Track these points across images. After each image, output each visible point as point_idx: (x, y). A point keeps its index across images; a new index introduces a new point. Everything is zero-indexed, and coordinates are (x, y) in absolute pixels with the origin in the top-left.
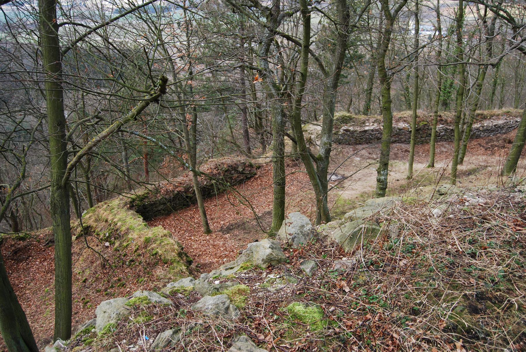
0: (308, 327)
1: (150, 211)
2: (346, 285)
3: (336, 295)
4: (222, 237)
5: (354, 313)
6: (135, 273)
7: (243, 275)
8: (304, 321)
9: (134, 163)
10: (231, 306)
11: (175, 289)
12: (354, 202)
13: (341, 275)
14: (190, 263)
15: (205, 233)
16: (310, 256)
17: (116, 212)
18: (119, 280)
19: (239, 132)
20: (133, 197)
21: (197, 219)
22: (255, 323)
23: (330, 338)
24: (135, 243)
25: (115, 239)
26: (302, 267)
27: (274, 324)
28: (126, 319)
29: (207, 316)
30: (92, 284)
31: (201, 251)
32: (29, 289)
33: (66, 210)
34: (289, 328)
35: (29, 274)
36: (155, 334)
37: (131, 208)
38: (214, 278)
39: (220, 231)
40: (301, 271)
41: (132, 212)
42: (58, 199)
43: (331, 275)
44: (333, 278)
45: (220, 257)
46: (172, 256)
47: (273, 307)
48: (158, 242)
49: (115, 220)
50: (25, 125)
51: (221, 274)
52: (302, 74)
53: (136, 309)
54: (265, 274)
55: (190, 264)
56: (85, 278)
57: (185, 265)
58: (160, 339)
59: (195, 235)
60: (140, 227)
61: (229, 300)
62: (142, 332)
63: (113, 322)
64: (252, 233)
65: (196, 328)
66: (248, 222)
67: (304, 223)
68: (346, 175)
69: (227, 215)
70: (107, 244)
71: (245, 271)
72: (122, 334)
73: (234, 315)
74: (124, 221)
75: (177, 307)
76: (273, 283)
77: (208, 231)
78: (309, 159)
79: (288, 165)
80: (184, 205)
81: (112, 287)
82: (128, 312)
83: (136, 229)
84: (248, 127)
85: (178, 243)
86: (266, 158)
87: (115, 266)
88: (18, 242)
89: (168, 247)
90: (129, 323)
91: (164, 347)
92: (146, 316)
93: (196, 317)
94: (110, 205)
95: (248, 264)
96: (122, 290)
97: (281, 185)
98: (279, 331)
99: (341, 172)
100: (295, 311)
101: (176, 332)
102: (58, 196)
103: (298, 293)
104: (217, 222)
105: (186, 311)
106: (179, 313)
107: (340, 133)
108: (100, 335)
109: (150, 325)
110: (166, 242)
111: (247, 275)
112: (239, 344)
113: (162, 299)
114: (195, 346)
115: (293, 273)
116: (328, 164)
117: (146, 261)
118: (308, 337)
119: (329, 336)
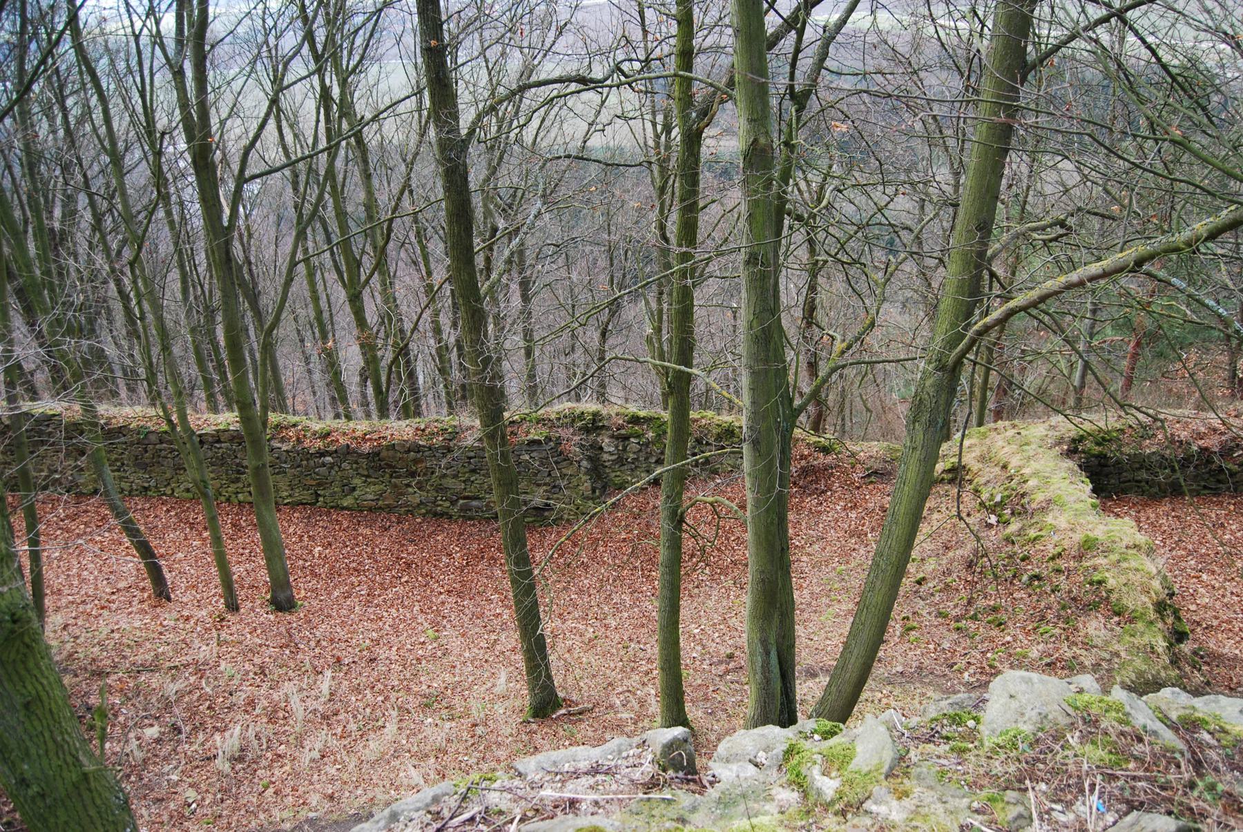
1: (1113, 475)
6: (1034, 608)
11: (1197, 715)
14: (1180, 636)
17: (1031, 453)
18: (995, 609)
21: (1233, 533)
24: (1056, 538)
25: (1013, 514)
28: (1058, 736)
30: (932, 595)
31: (1217, 618)
32: (809, 555)
33: (940, 421)
35: (817, 524)
36: (1124, 807)
37: (1071, 453)
41: (1070, 464)
42: (932, 391)
48: (1114, 557)
49: (1026, 471)
53: (1090, 724)
56: (922, 575)
57: (1164, 637)
59: (1213, 572)
60: (1079, 506)
62: (1093, 786)
63: (1027, 728)
70: (993, 519)
72: (1041, 766)
74: (1046, 481)
75: (1198, 765)
81: (974, 618)
82: (1068, 720)
83: (1068, 505)
85: (1165, 577)
89: (1136, 578)
90: (1063, 747)
92: (1111, 752)
94: (1023, 432)
102: (932, 386)
105: (1220, 787)
106: (1200, 784)
108: (988, 744)
109: (1114, 778)
110: (1133, 564)
117: (1070, 591)
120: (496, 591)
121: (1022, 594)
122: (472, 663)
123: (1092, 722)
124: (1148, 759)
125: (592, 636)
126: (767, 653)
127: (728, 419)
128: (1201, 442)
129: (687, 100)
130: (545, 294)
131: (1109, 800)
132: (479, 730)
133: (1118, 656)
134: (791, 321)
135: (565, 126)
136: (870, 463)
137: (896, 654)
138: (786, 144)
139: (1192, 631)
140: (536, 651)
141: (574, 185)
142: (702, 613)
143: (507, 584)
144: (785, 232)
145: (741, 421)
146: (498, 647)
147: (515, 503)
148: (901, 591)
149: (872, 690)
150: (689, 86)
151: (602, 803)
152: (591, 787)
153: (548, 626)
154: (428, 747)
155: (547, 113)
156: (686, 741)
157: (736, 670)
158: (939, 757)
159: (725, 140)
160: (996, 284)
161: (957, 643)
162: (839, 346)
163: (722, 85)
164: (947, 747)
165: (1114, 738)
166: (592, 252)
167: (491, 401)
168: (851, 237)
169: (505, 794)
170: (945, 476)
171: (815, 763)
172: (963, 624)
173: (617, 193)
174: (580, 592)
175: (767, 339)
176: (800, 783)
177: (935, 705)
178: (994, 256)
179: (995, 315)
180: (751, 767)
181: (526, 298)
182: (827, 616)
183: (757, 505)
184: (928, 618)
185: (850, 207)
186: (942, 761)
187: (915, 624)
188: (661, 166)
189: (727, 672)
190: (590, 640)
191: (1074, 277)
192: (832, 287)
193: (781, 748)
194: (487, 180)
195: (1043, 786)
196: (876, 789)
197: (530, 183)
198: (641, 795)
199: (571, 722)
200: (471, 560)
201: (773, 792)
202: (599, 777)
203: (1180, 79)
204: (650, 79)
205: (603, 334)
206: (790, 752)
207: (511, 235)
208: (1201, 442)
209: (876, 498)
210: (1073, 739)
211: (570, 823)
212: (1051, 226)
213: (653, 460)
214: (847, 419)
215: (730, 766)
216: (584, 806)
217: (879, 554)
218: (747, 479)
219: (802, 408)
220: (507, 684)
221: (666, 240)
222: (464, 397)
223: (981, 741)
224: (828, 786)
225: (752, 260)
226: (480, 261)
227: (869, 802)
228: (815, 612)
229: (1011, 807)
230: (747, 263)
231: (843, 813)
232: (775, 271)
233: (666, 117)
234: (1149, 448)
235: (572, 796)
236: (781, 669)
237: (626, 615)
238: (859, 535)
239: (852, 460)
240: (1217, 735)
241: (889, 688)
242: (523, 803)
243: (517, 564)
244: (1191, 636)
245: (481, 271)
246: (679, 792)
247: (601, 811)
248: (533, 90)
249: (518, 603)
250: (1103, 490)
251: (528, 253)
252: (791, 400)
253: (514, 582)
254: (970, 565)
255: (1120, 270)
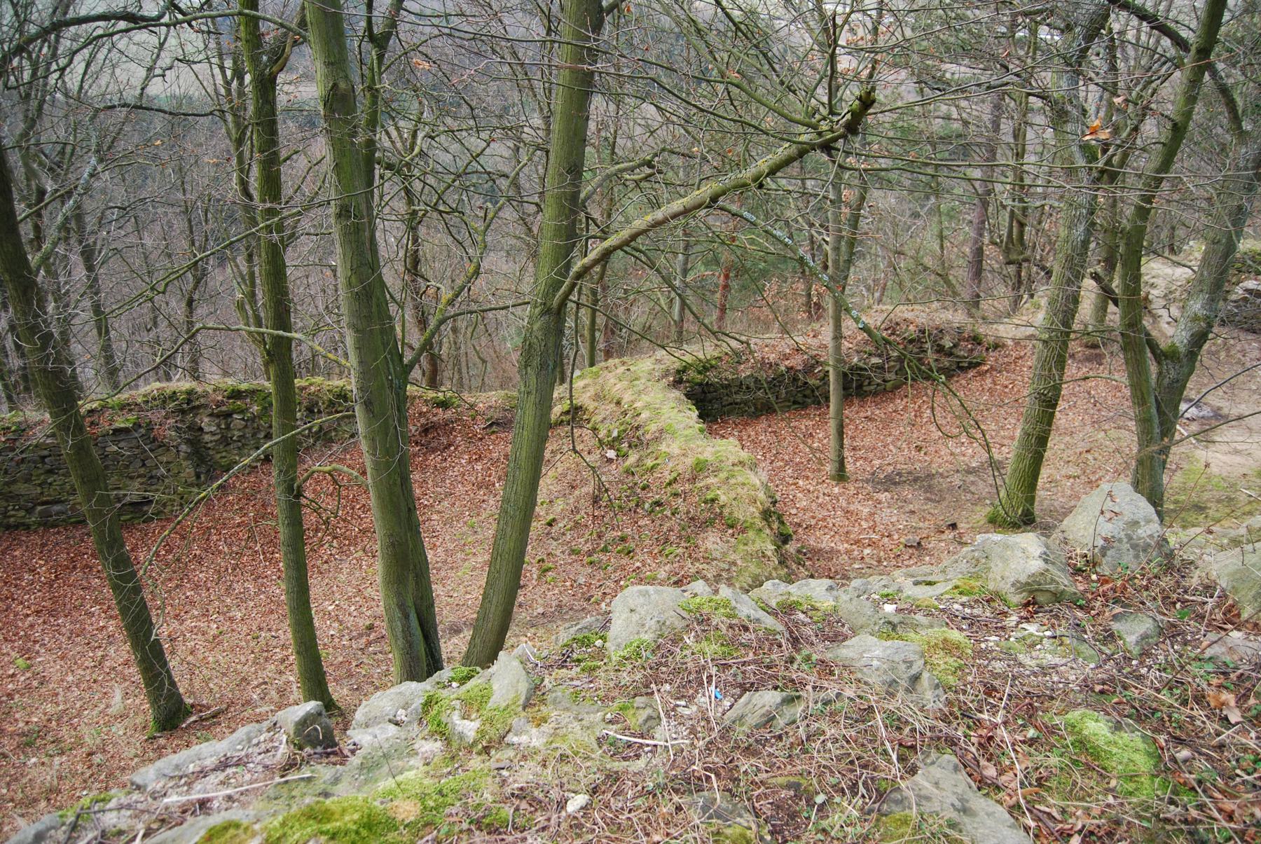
0: (1113, 783)
1: (714, 400)
2: (1233, 703)
3: (1198, 723)
4: (869, 497)
5: (1244, 783)
6: (658, 533)
7: (956, 606)
8: (1106, 763)
9: (702, 282)
10: (926, 675)
12: (1232, 486)
13: (1223, 673)
14: (785, 539)
15: (833, 478)
16: (1143, 603)
17: (642, 387)
18: (623, 539)
19: (959, 253)
20: (688, 358)
21: (820, 441)
22: (980, 732)
23: (1168, 827)
24: (671, 465)
25: (630, 446)
26: (1116, 626)
27: (1026, 747)
29: (866, 683)
30: (564, 534)
33: (551, 363)
34: (1062, 769)
35: (443, 481)
36: (738, 691)
37: (677, 383)
38: (882, 596)
39: (867, 481)
40: (1112, 635)
41: (677, 394)
42: (540, 335)
43: (1193, 668)
44: (1198, 676)
45: (857, 542)
46: (748, 513)
47: (1029, 707)
48: (723, 475)
49: (638, 404)
50: (488, 163)
51: (900, 590)
52: (1175, 125)
54: (1015, 618)
55: (785, 542)
56: (551, 517)
58: (750, 706)
59: (807, 478)
61: (922, 661)
63: (648, 637)
64: (945, 504)
65: (839, 705)
66: (941, 475)
67: (1140, 516)
68: (1225, 411)
69: (891, 447)
70: (611, 454)
71: (964, 599)
72: (664, 669)
73: (932, 699)
74: (657, 412)
75: (795, 641)
76: (1033, 645)
77: (841, 475)
78: (1142, 352)
79: (1072, 356)
80: (795, 402)
81: (605, 550)
82: (684, 623)
84: (986, 241)
86: (1022, 324)
87: (620, 507)
88: (435, 410)
89: (742, 492)
91: (757, 727)
93: (840, 677)
95: (973, 583)
96: (624, 562)
97: (1048, 403)
98: (1037, 769)
99: (1216, 400)
100: (1085, 732)
101: (790, 701)
102: (539, 329)
103: (1098, 688)
104: (865, 459)
105: (814, 657)
106: (799, 658)
107: (1234, 297)
110: (740, 479)
111: (967, 610)
112: (935, 771)
113: (761, 614)
114: (829, 745)
115: (1090, 635)
116: (1190, 373)
117: (688, 512)
118: (1108, 806)
119: (1167, 820)
120: (96, 602)
121: (646, 521)
122: (77, 686)
123: (704, 621)
124: (754, 645)
125: (216, 632)
126: (406, 616)
127: (340, 383)
128: (787, 363)
129: (255, 39)
130: (115, 263)
131: (724, 687)
132: (97, 759)
133: (734, 563)
134: (392, 277)
135: (118, 71)
136: (490, 413)
137: (535, 596)
138: (370, 88)
139: (795, 532)
140: (152, 660)
141: (136, 139)
142: (335, 588)
143: (107, 592)
144: (377, 183)
145: (351, 384)
146: (108, 664)
147: (104, 501)
148: (533, 534)
149: (516, 636)
150: (257, 27)
151: (236, 797)
152: (222, 783)
153: (163, 630)
154: (36, 791)
155: (92, 57)
156: (320, 714)
157: (377, 640)
158: (572, 679)
159: (301, 87)
160: (592, 226)
161: (591, 576)
162: (446, 294)
163: (293, 26)
164: (578, 669)
165: (724, 631)
166: (166, 214)
167: (62, 393)
168: (449, 186)
169: (123, 812)
170: (563, 418)
171: (454, 709)
172: (595, 558)
173: (190, 147)
174: (197, 587)
175: (369, 298)
176: (442, 732)
177: (565, 634)
178: (588, 197)
179: (592, 256)
180: (392, 726)
181: (90, 268)
182: (464, 572)
183: (377, 467)
184: (562, 557)
185: (446, 155)
186: (575, 683)
187: (550, 565)
188: (234, 115)
189: (369, 644)
190: (215, 637)
191: (659, 215)
192: (434, 239)
193: (418, 703)
194: (25, 135)
195: (667, 687)
196: (515, 721)
197: (79, 137)
198: (278, 780)
199: (204, 728)
200: (60, 572)
201: (416, 746)
202: (230, 771)
203: (742, 27)
204: (213, 18)
205: (190, 303)
206: (429, 703)
207: (64, 198)
208: (787, 363)
209: (499, 448)
210: (689, 640)
211: (202, 823)
212: (639, 166)
213: (262, 435)
214: (464, 370)
215: (370, 730)
216: (216, 804)
217: (506, 500)
218: (363, 442)
219: (416, 360)
220: (124, 700)
221: (250, 197)
222: (27, 389)
223: (609, 657)
224: (469, 728)
225: (343, 213)
226: (26, 231)
227: (510, 735)
228: (452, 568)
229: (641, 711)
230: (339, 216)
231: (486, 750)
232: (370, 223)
233: (235, 62)
234: (745, 372)
235: (201, 796)
236: (423, 630)
237: (252, 604)
238: (487, 486)
239: (472, 412)
240: (810, 613)
241: (533, 630)
242: (146, 816)
243: (116, 567)
244: (794, 537)
245: (31, 241)
246: (319, 767)
247: (236, 804)
248: (72, 29)
249: (124, 611)
250: (708, 416)
251: (87, 219)
252: (401, 357)
253: (115, 588)
254: (596, 500)
255: (698, 206)
